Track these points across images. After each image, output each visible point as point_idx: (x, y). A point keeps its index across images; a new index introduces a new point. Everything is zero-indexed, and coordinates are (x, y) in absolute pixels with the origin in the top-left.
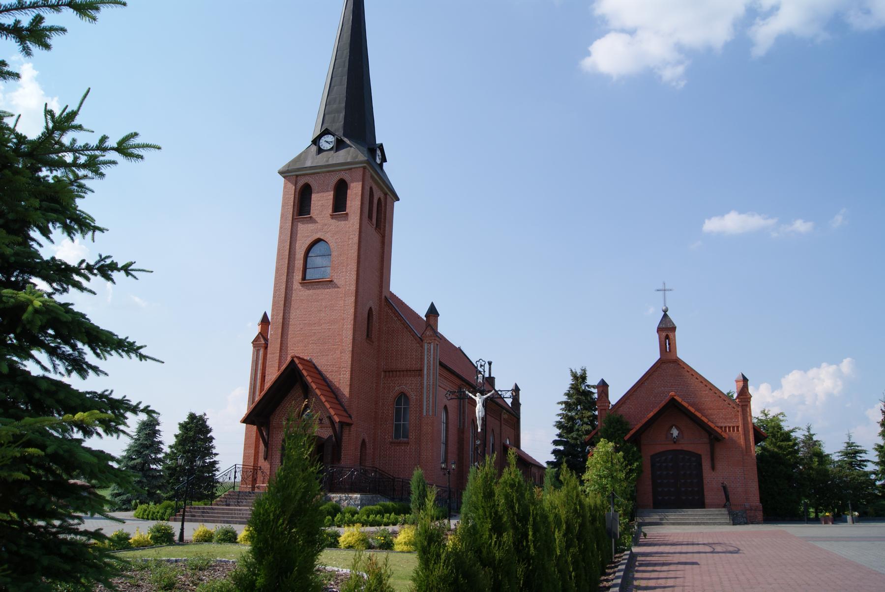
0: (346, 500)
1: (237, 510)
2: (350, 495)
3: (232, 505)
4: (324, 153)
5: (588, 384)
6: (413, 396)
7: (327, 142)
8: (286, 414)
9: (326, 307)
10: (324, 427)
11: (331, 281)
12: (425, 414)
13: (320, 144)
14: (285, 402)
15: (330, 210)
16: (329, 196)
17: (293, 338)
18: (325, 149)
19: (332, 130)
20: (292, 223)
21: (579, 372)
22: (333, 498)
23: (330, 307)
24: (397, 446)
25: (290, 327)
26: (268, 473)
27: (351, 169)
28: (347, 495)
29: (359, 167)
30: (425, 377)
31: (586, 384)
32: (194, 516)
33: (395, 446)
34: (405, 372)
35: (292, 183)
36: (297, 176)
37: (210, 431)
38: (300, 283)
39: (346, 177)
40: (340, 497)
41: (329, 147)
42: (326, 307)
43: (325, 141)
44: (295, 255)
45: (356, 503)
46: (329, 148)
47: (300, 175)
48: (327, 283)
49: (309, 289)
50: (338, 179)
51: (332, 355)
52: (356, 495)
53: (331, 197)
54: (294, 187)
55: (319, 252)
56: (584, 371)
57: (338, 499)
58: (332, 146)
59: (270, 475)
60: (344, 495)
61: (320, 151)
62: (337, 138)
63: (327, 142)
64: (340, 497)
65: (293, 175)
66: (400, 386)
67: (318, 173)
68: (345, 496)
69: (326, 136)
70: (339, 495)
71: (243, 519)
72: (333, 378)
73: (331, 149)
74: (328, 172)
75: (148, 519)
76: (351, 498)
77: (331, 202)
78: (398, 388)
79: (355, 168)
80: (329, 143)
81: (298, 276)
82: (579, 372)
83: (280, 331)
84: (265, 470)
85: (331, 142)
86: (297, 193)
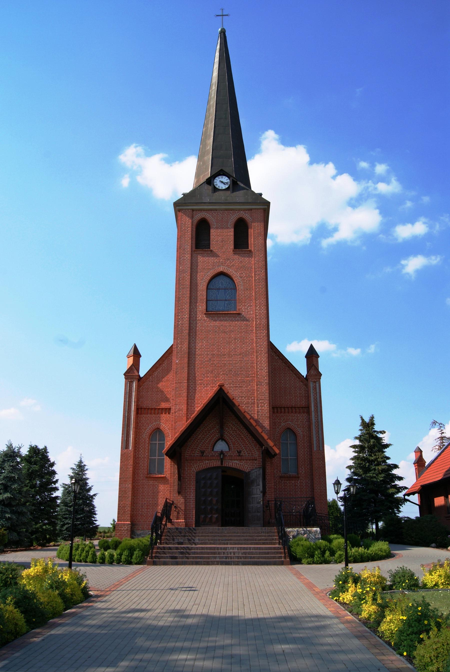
0: (304, 534)
1: (221, 548)
2: (308, 529)
3: (198, 544)
4: (220, 192)
5: (376, 430)
6: (300, 432)
7: (222, 182)
8: (199, 446)
9: (235, 339)
10: (243, 460)
11: (239, 314)
12: (315, 449)
13: (215, 184)
14: (198, 434)
15: (231, 246)
16: (230, 233)
17: (201, 368)
18: (220, 188)
19: (227, 170)
20: (191, 254)
21: (367, 420)
22: (290, 532)
23: (240, 339)
24: (287, 480)
25: (198, 357)
26: (183, 508)
27: (251, 210)
28: (305, 529)
29: (260, 209)
30: (313, 414)
31: (374, 430)
32: (176, 558)
33: (285, 480)
34: (290, 409)
35: (188, 217)
36: (193, 210)
37: (53, 464)
38: (205, 314)
39: (247, 216)
40: (298, 531)
41: (224, 187)
42: (235, 339)
43: (220, 181)
44: (197, 285)
45: (317, 536)
46: (224, 188)
47: (197, 210)
48: (235, 315)
49: (215, 321)
50: (238, 217)
51: (247, 387)
52: (315, 529)
53: (232, 233)
54: (190, 221)
55: (220, 285)
56: (372, 418)
57: (295, 533)
58: (227, 186)
59: (185, 510)
60: (301, 529)
61: (215, 190)
62: (233, 180)
63: (222, 182)
64: (298, 531)
65: (188, 209)
66: (286, 422)
67: (216, 210)
68: (304, 530)
69: (220, 177)
70: (296, 529)
71: (241, 559)
72: (249, 410)
73: (227, 189)
74: (227, 210)
75: (129, 563)
76: (310, 532)
77: (232, 238)
78: (284, 424)
79: (255, 209)
80: (224, 184)
81: (201, 307)
82: (367, 420)
83: (186, 360)
84: (179, 505)
85: (227, 183)
86: (194, 227)
